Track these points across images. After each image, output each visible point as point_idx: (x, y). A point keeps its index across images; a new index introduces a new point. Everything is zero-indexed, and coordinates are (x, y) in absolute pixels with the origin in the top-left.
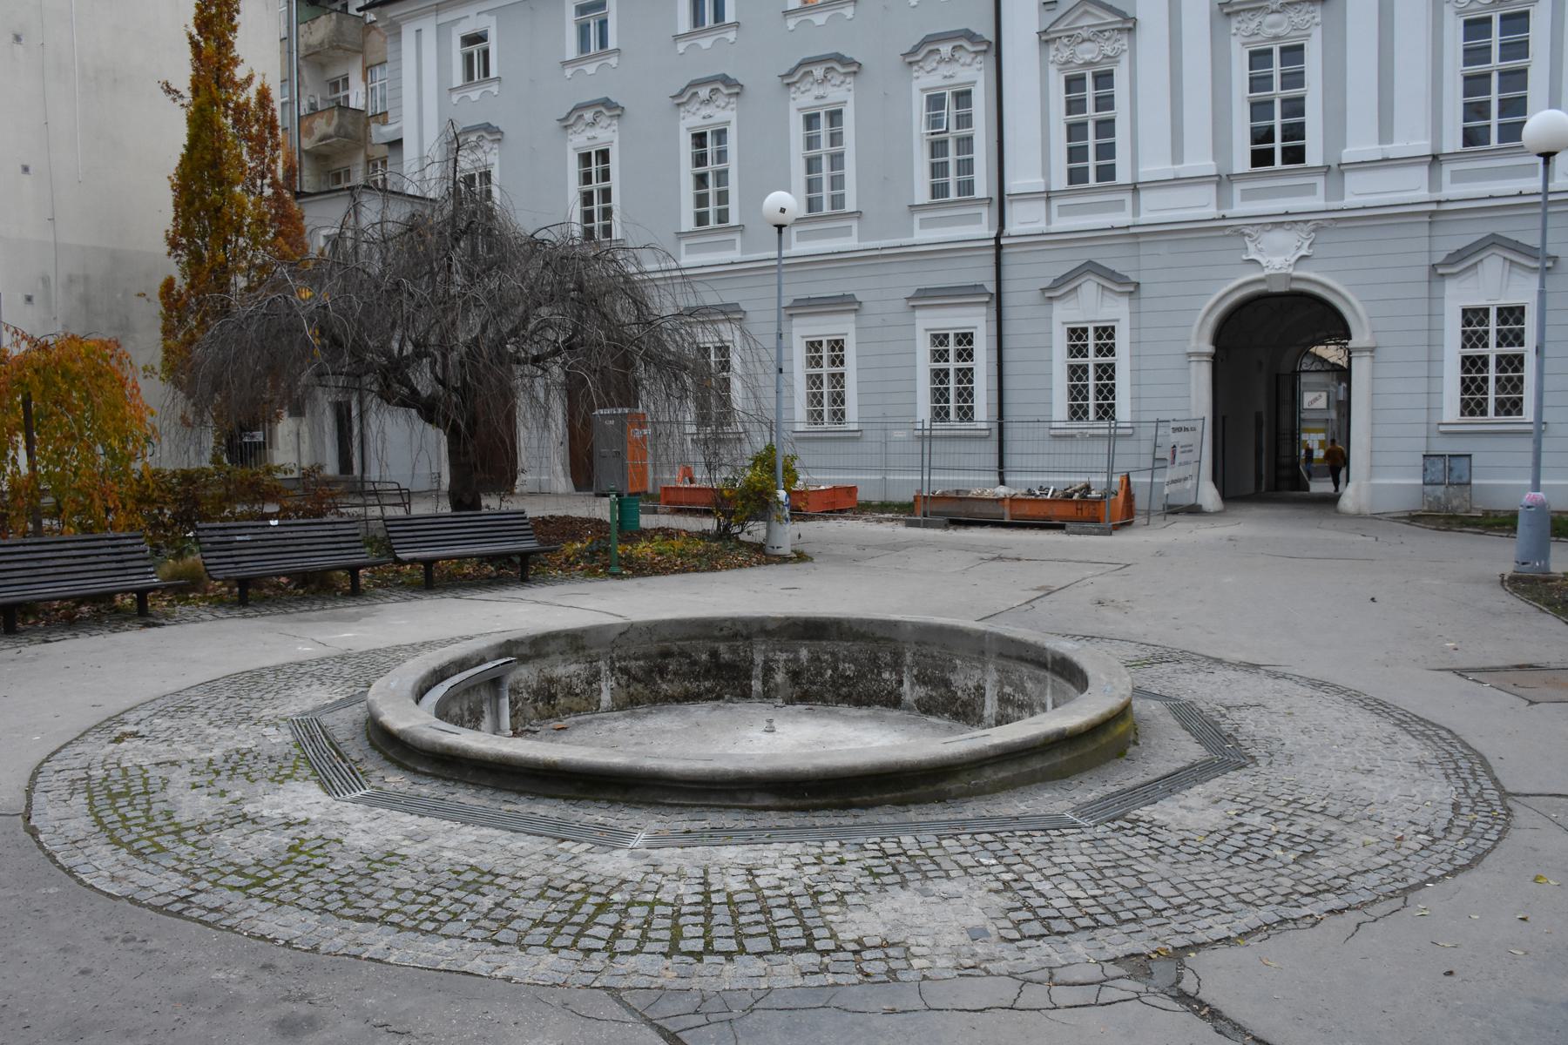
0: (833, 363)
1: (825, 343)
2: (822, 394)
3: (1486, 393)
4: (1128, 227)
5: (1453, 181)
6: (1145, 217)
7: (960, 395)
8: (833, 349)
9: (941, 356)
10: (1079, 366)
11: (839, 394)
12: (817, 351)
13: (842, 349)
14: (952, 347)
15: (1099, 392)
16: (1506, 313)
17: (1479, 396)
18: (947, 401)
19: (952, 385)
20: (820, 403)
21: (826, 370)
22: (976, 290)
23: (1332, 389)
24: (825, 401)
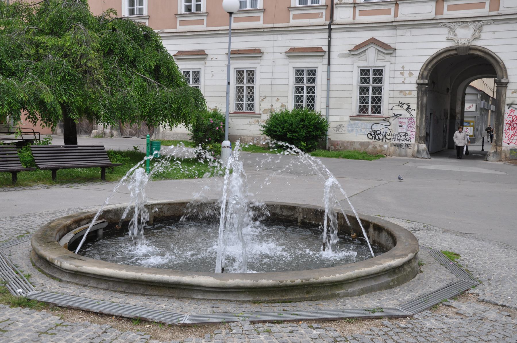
0: (249, 81)
1: (245, 72)
2: (243, 96)
3: (243, 102)
4: (392, 22)
5: (448, 10)
6: (400, 17)
7: (308, 99)
8: (249, 75)
9: (300, 80)
10: (365, 87)
11: (251, 96)
12: (241, 75)
13: (253, 75)
14: (305, 76)
15: (374, 100)
16: (376, 71)
17: (241, 102)
18: (302, 102)
19: (305, 94)
20: (242, 100)
21: (245, 84)
22: (318, 49)
23: (478, 102)
24: (244, 99)
